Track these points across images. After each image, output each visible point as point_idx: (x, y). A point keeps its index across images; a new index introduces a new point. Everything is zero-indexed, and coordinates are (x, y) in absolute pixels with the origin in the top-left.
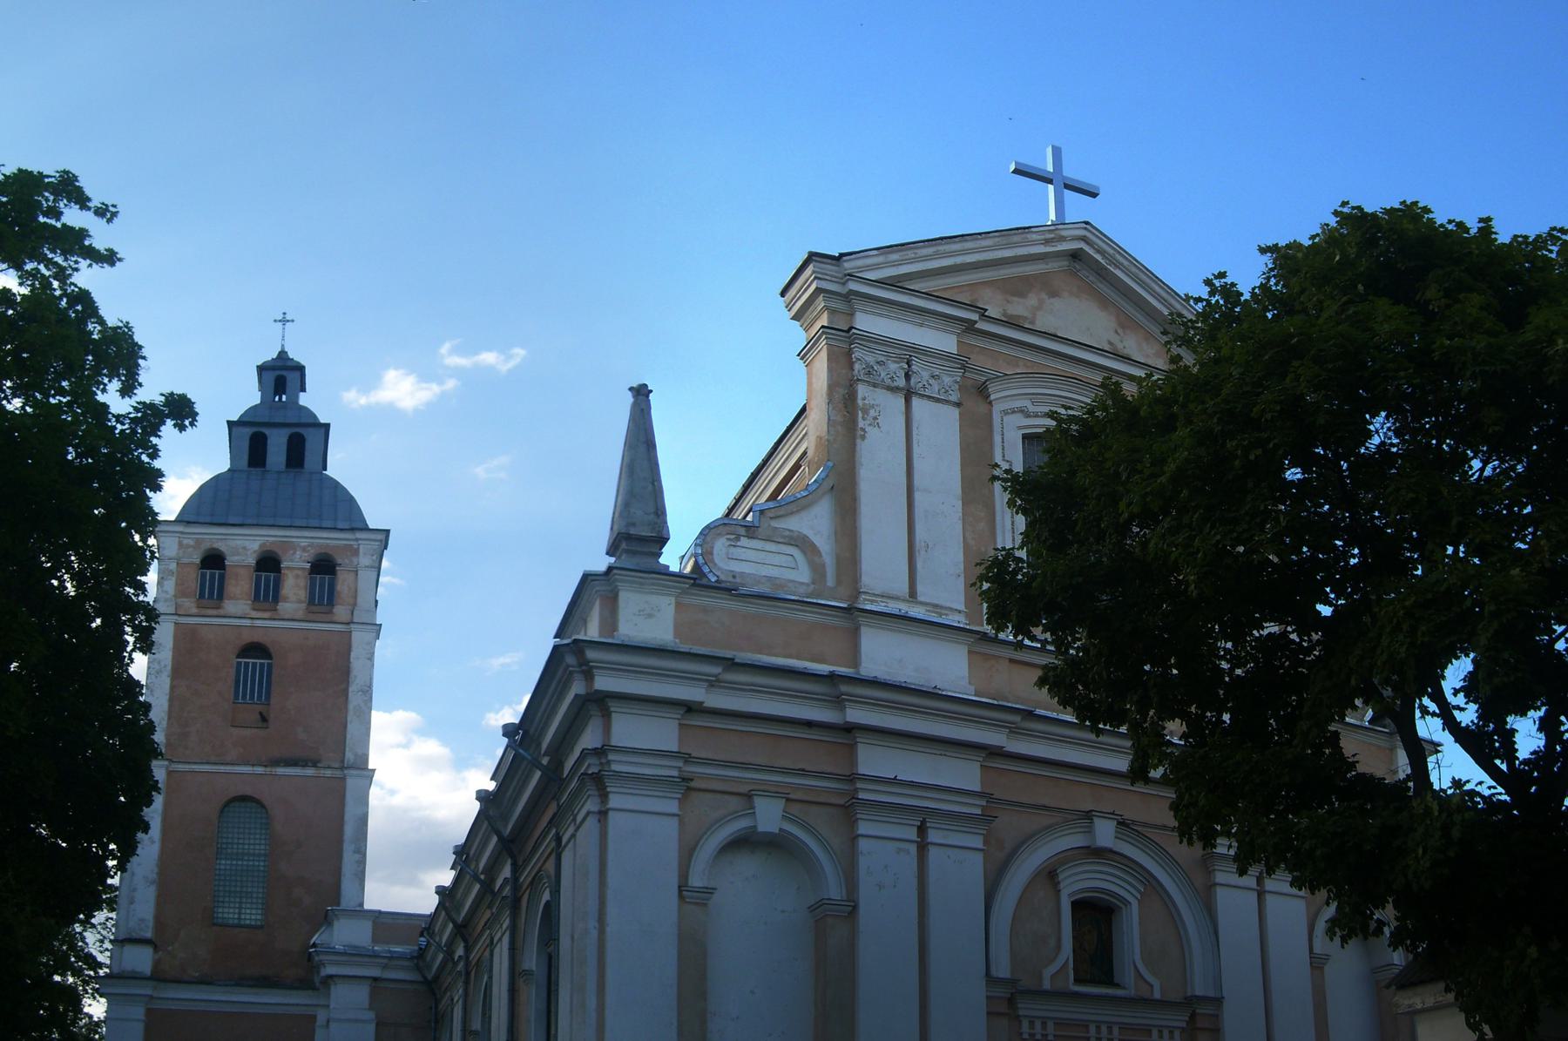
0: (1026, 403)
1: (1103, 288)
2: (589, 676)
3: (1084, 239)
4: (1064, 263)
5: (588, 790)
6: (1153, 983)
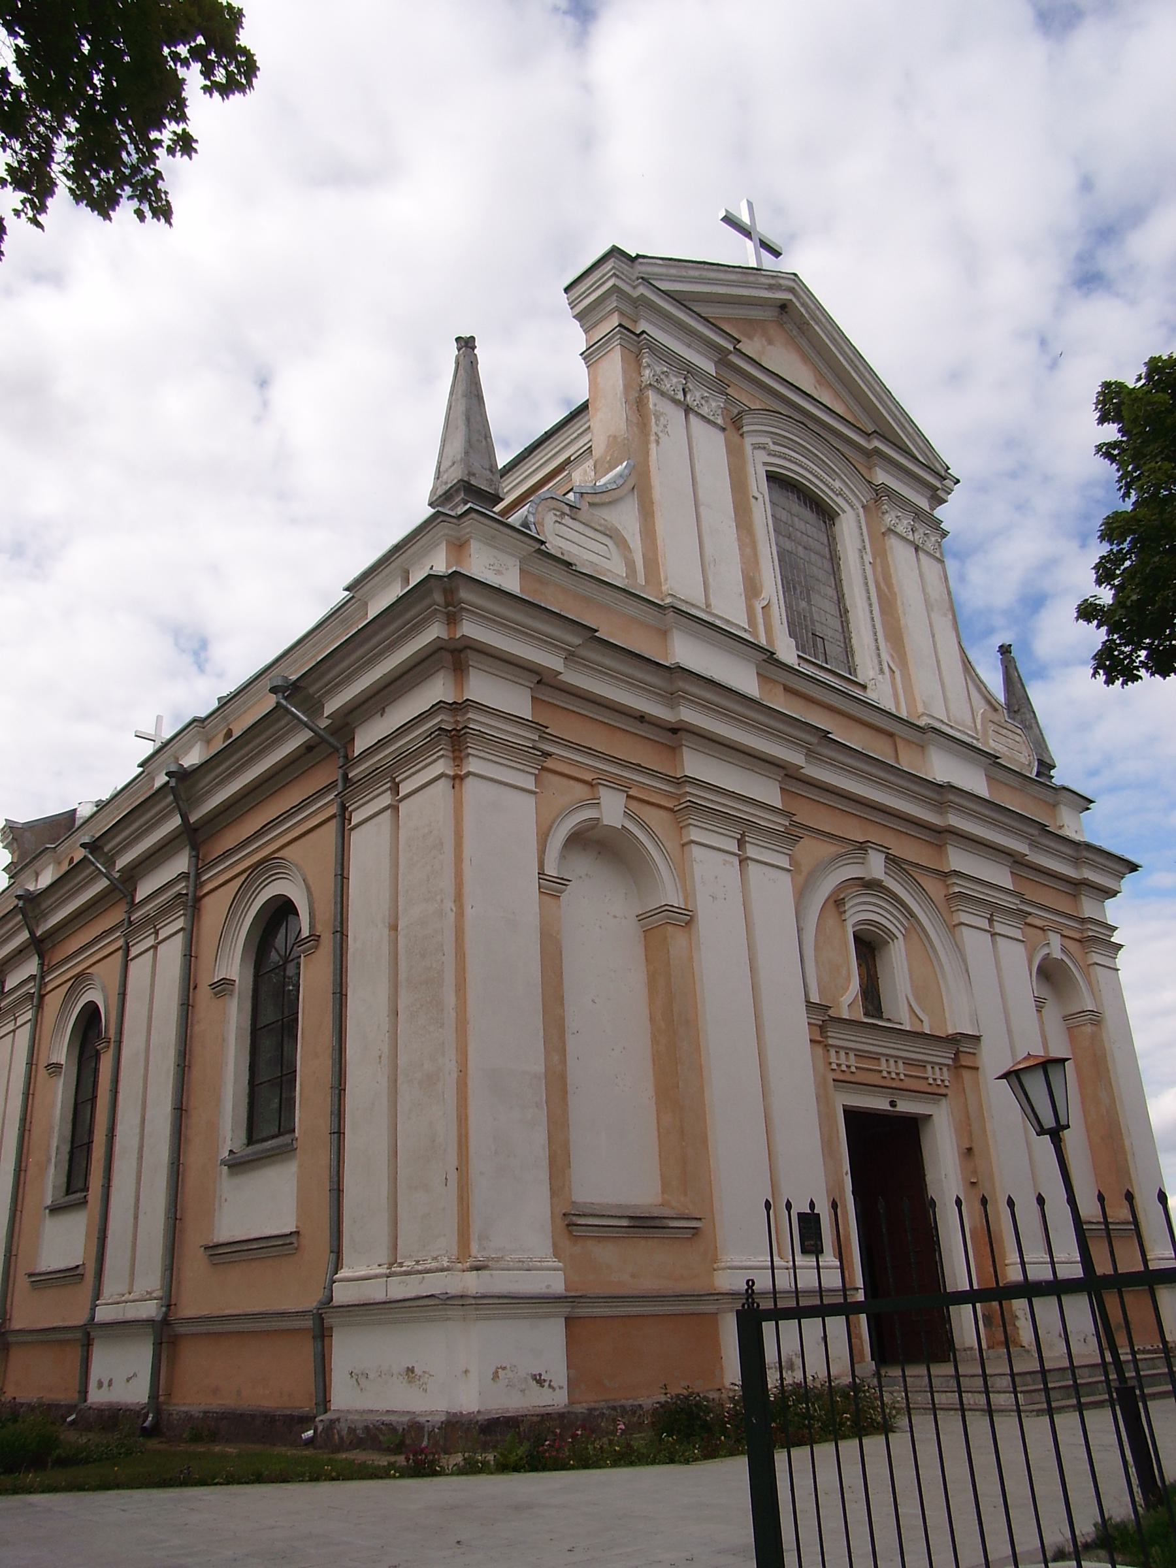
0: (768, 440)
1: (803, 343)
2: (452, 620)
3: (792, 290)
4: (770, 314)
5: (441, 749)
6: (923, 1019)
